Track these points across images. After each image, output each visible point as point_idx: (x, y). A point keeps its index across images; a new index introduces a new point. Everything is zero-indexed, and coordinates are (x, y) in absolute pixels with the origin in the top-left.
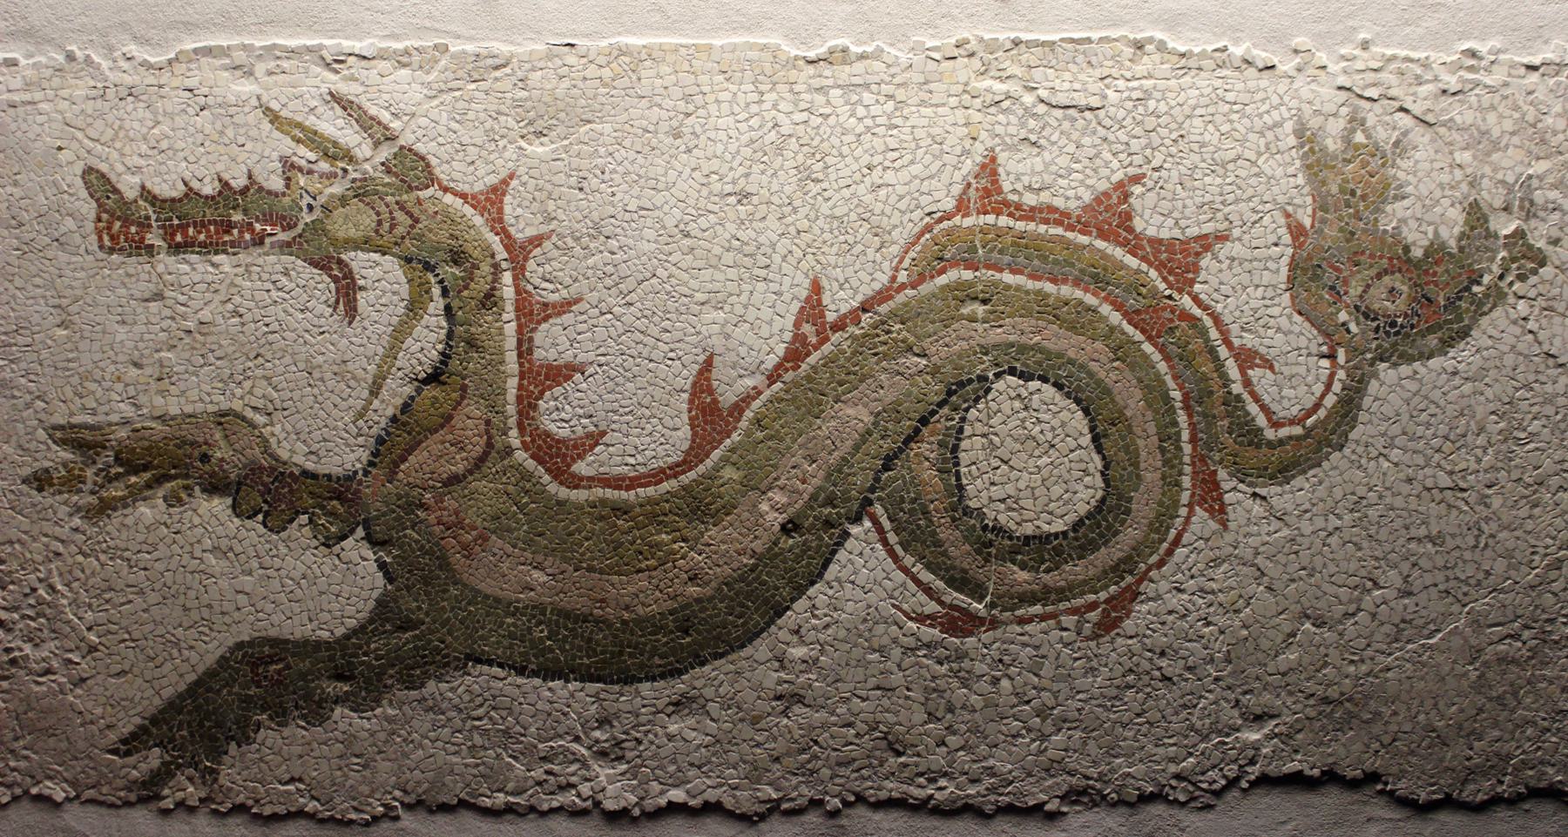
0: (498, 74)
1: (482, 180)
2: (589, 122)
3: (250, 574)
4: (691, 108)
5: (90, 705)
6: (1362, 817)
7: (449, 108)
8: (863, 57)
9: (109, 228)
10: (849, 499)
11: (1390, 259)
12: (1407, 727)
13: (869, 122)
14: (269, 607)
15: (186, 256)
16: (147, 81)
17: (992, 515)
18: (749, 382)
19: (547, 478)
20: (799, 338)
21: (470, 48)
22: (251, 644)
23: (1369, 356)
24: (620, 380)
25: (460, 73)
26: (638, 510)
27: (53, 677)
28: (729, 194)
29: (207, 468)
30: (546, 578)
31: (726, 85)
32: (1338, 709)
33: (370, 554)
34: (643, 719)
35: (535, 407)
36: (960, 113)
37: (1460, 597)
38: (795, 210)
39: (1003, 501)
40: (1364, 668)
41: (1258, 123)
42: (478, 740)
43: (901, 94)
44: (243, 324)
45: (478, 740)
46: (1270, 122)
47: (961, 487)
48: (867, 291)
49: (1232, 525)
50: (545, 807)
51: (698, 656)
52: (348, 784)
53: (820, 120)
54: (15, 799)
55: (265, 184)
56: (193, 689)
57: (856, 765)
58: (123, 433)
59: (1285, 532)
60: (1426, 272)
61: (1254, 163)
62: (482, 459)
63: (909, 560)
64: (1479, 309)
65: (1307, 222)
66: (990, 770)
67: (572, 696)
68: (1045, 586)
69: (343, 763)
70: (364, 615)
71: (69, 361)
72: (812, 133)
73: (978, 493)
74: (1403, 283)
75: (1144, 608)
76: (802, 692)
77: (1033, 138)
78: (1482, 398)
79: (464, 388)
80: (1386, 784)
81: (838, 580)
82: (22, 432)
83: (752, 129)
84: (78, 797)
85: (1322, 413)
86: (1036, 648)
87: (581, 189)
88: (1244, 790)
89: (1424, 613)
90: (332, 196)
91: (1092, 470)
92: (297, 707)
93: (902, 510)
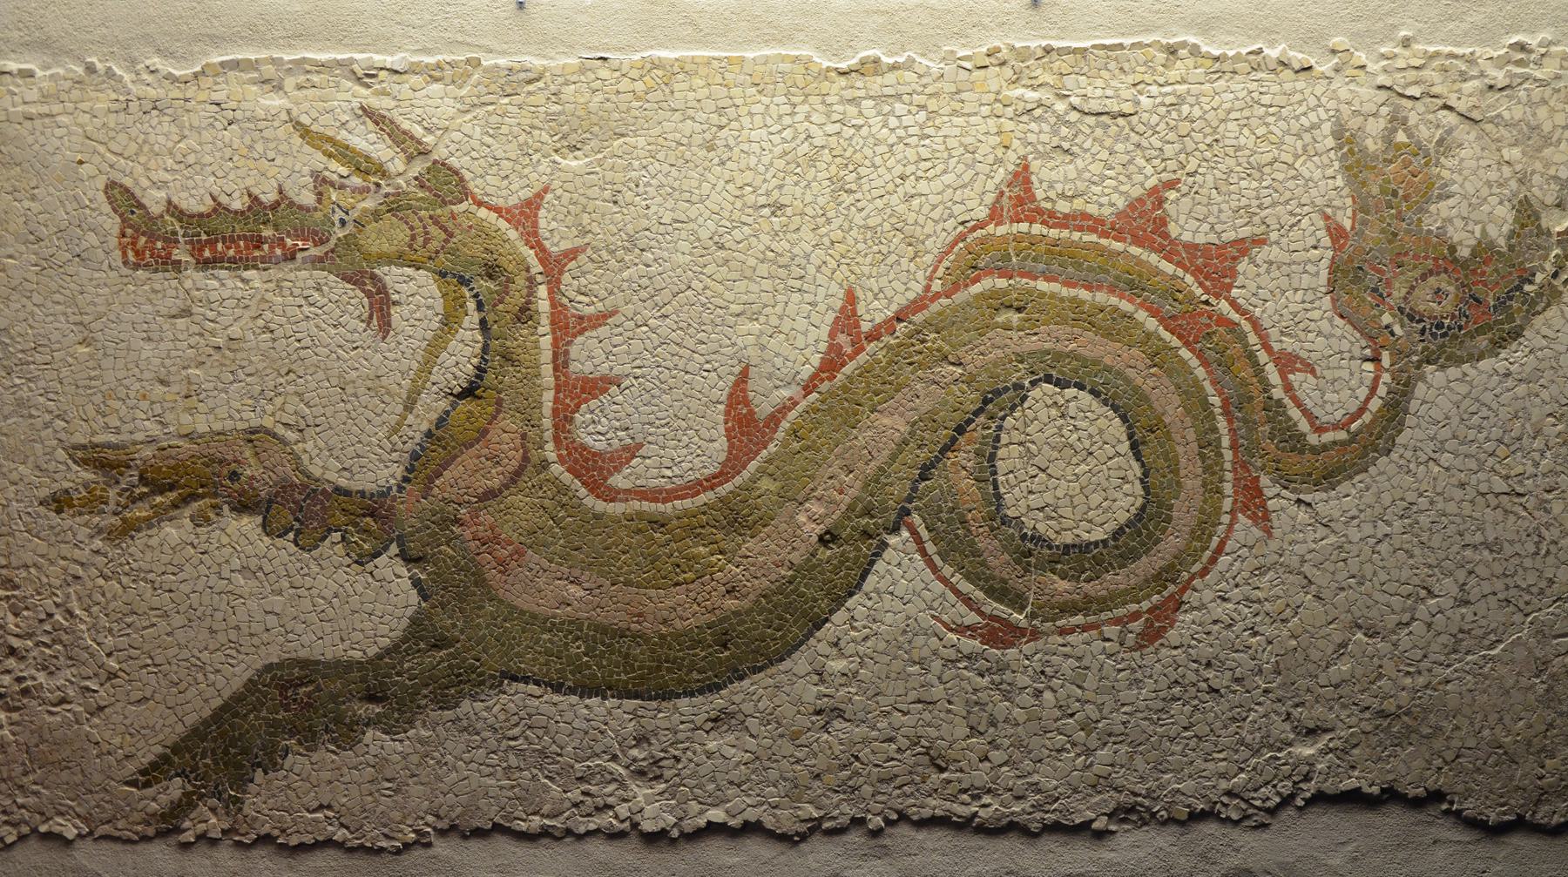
0: (531, 88)
1: (517, 193)
2: (623, 135)
3: (280, 593)
4: (724, 121)
5: (107, 735)
6: (1428, 840)
7: (482, 122)
8: (894, 67)
9: (134, 244)
10: (886, 510)
11: (1436, 259)
12: (1471, 743)
13: (901, 132)
14: (300, 628)
15: (215, 272)
16: (172, 95)
17: (1030, 524)
18: (785, 393)
19: (583, 491)
20: (834, 348)
21: (503, 62)
22: (280, 666)
23: (1415, 358)
24: (656, 392)
25: (493, 88)
26: (675, 522)
27: (68, 707)
28: (763, 206)
29: (236, 486)
30: (583, 593)
31: (758, 97)
32: (1395, 723)
33: (404, 571)
34: (681, 736)
35: (571, 420)
36: (991, 122)
37: (1522, 605)
38: (829, 221)
39: (1041, 509)
40: (1421, 680)
41: (1295, 126)
42: (513, 760)
43: (932, 105)
44: (274, 340)
45: (513, 760)
46: (1307, 124)
47: (999, 497)
48: (900, 301)
49: (1276, 532)
50: (582, 830)
51: (737, 670)
52: (379, 810)
53: (853, 131)
54: (22, 838)
55: (296, 199)
56: (217, 715)
57: (898, 782)
58: (148, 452)
59: (1332, 539)
60: (1474, 272)
61: (1291, 166)
62: (518, 473)
63: (947, 571)
64: (1533, 308)
65: (1347, 224)
66: (1036, 788)
67: (610, 713)
68: (1086, 595)
69: (373, 788)
70: (398, 633)
71: (91, 379)
72: (845, 144)
73: (1016, 501)
74: (1449, 284)
75: (1189, 617)
76: (842, 706)
77: (1066, 145)
78: (1538, 400)
79: (499, 402)
80: (1452, 803)
81: (877, 591)
82: (40, 452)
83: (785, 141)
84: (91, 833)
85: (1367, 417)
86: (1079, 659)
87: (615, 202)
88: (1300, 809)
89: (1484, 622)
90: (365, 210)
91: (1131, 478)
92: (327, 731)
93: (939, 519)
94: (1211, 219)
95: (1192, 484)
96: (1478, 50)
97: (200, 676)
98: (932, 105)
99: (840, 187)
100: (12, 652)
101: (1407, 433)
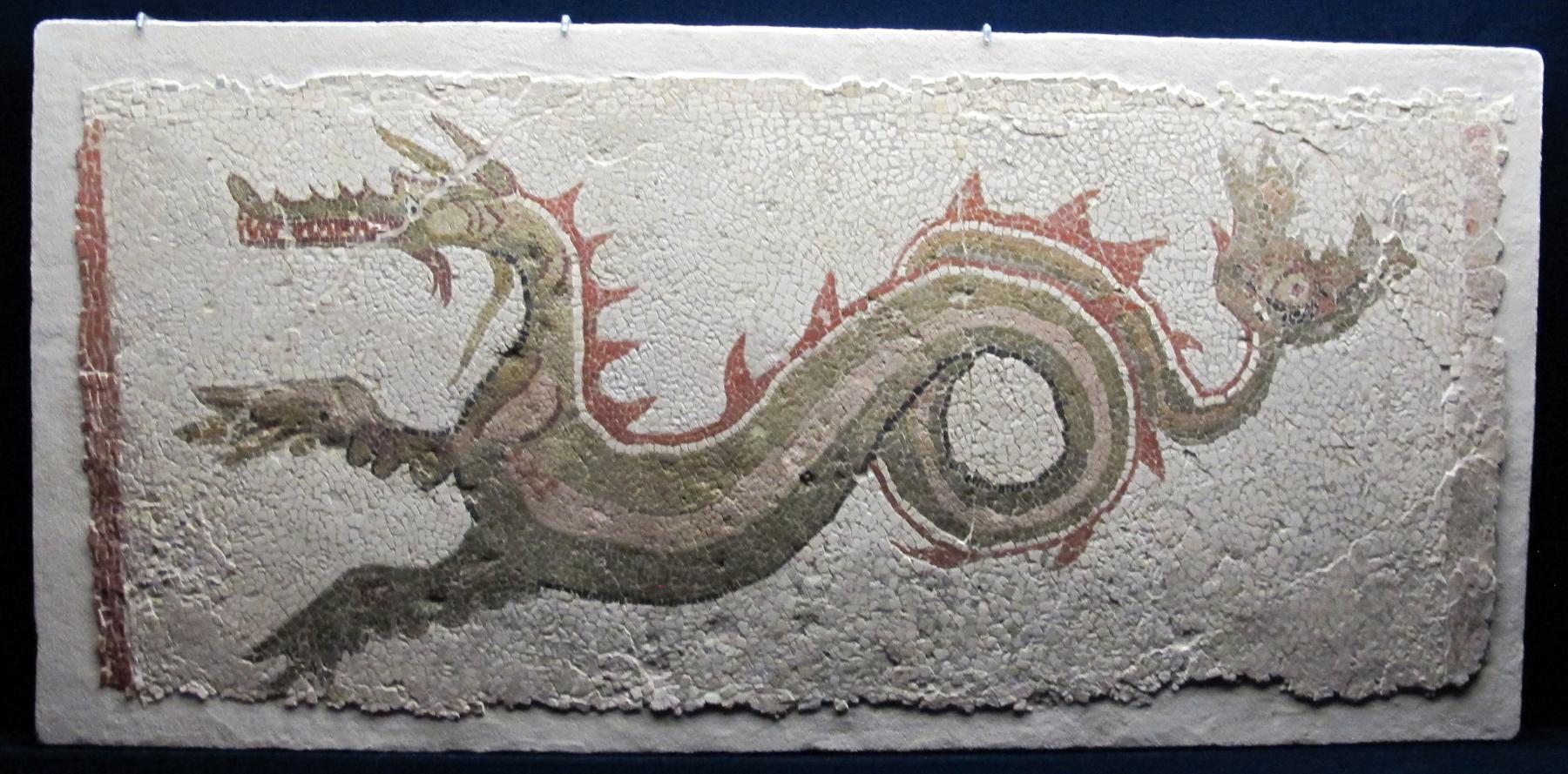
0: (570, 101)
1: (554, 192)
3: (360, 511)
4: (729, 131)
6: (1268, 713)
8: (871, 91)
10: (856, 455)
12: (1305, 639)
13: (875, 144)
14: (377, 540)
17: (972, 466)
20: (816, 322)
21: (548, 79)
22: (362, 570)
23: (1278, 339)
24: (668, 354)
25: (540, 101)
29: (326, 424)
32: (1250, 626)
33: (459, 497)
35: (597, 376)
36: (950, 138)
39: (982, 456)
40: (1271, 592)
41: (1190, 150)
43: (901, 122)
45: (548, 650)
46: (1200, 149)
47: (948, 445)
48: (871, 284)
49: (1167, 477)
50: (603, 707)
55: (377, 191)
57: (860, 672)
58: (257, 395)
59: (1210, 482)
63: (905, 504)
65: (1229, 231)
66: (971, 678)
73: (962, 450)
75: (1097, 544)
77: (1009, 159)
79: (539, 361)
81: (847, 521)
83: (778, 148)
85: (1240, 386)
86: (1009, 577)
88: (1175, 692)
94: (1124, 223)
95: (1103, 437)
96: (1328, 97)
97: (298, 577)
98: (901, 122)
99: (823, 187)
100: (156, 551)
101: (1270, 397)
